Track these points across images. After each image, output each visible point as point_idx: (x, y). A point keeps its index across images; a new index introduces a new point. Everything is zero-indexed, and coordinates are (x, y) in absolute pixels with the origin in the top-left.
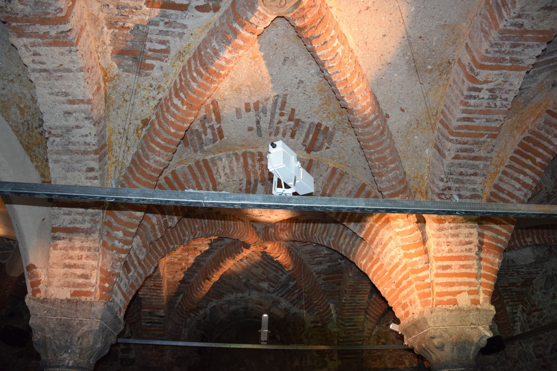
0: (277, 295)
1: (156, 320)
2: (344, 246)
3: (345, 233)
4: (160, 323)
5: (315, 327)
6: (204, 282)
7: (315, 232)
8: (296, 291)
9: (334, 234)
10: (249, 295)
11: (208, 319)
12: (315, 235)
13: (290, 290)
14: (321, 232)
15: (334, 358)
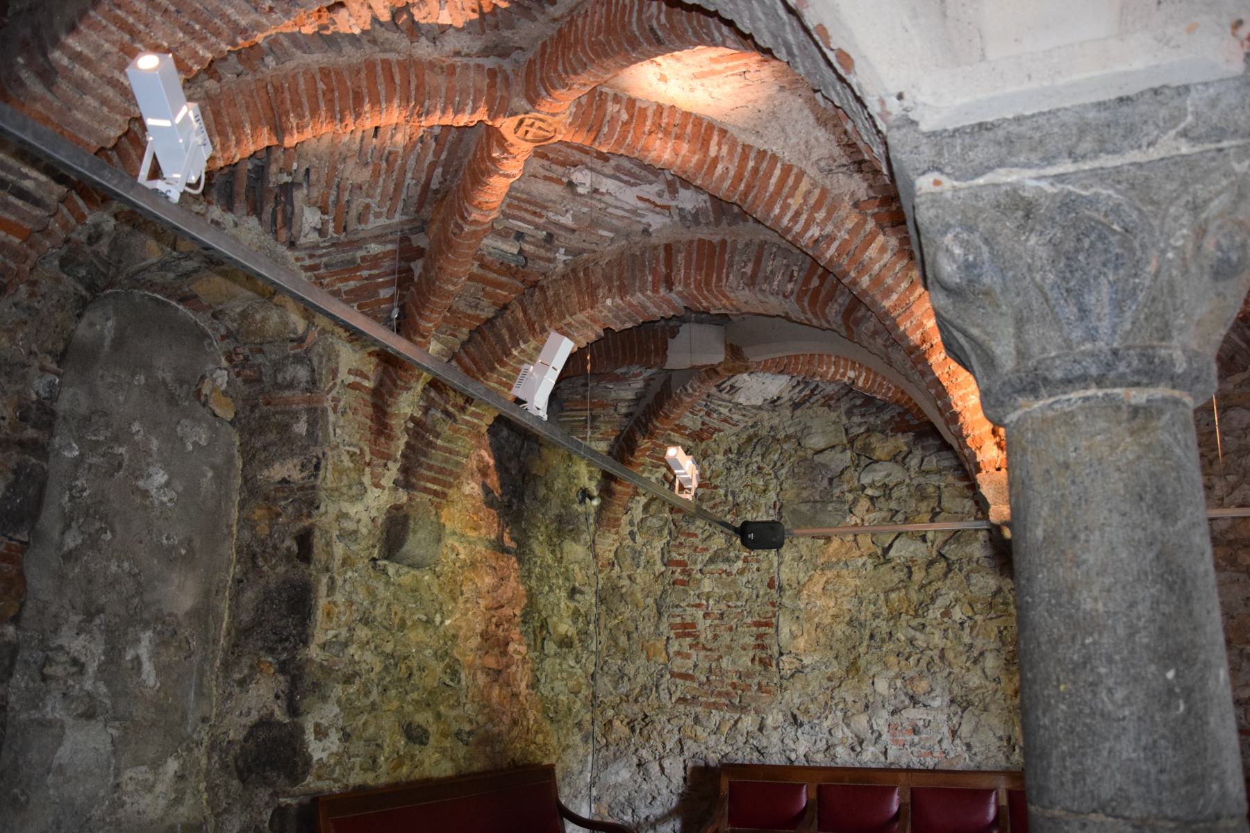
0: (297, 259)
1: (28, 184)
2: (877, 267)
3: (881, 239)
4: (37, 202)
5: (354, 386)
6: (254, 129)
7: (791, 194)
8: (365, 273)
9: (849, 225)
10: (236, 225)
11: (103, 247)
12: (790, 201)
13: (353, 261)
14: (812, 202)
15: (383, 482)
